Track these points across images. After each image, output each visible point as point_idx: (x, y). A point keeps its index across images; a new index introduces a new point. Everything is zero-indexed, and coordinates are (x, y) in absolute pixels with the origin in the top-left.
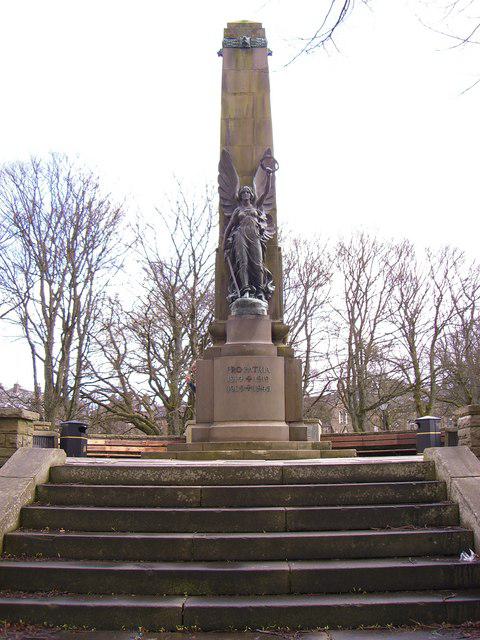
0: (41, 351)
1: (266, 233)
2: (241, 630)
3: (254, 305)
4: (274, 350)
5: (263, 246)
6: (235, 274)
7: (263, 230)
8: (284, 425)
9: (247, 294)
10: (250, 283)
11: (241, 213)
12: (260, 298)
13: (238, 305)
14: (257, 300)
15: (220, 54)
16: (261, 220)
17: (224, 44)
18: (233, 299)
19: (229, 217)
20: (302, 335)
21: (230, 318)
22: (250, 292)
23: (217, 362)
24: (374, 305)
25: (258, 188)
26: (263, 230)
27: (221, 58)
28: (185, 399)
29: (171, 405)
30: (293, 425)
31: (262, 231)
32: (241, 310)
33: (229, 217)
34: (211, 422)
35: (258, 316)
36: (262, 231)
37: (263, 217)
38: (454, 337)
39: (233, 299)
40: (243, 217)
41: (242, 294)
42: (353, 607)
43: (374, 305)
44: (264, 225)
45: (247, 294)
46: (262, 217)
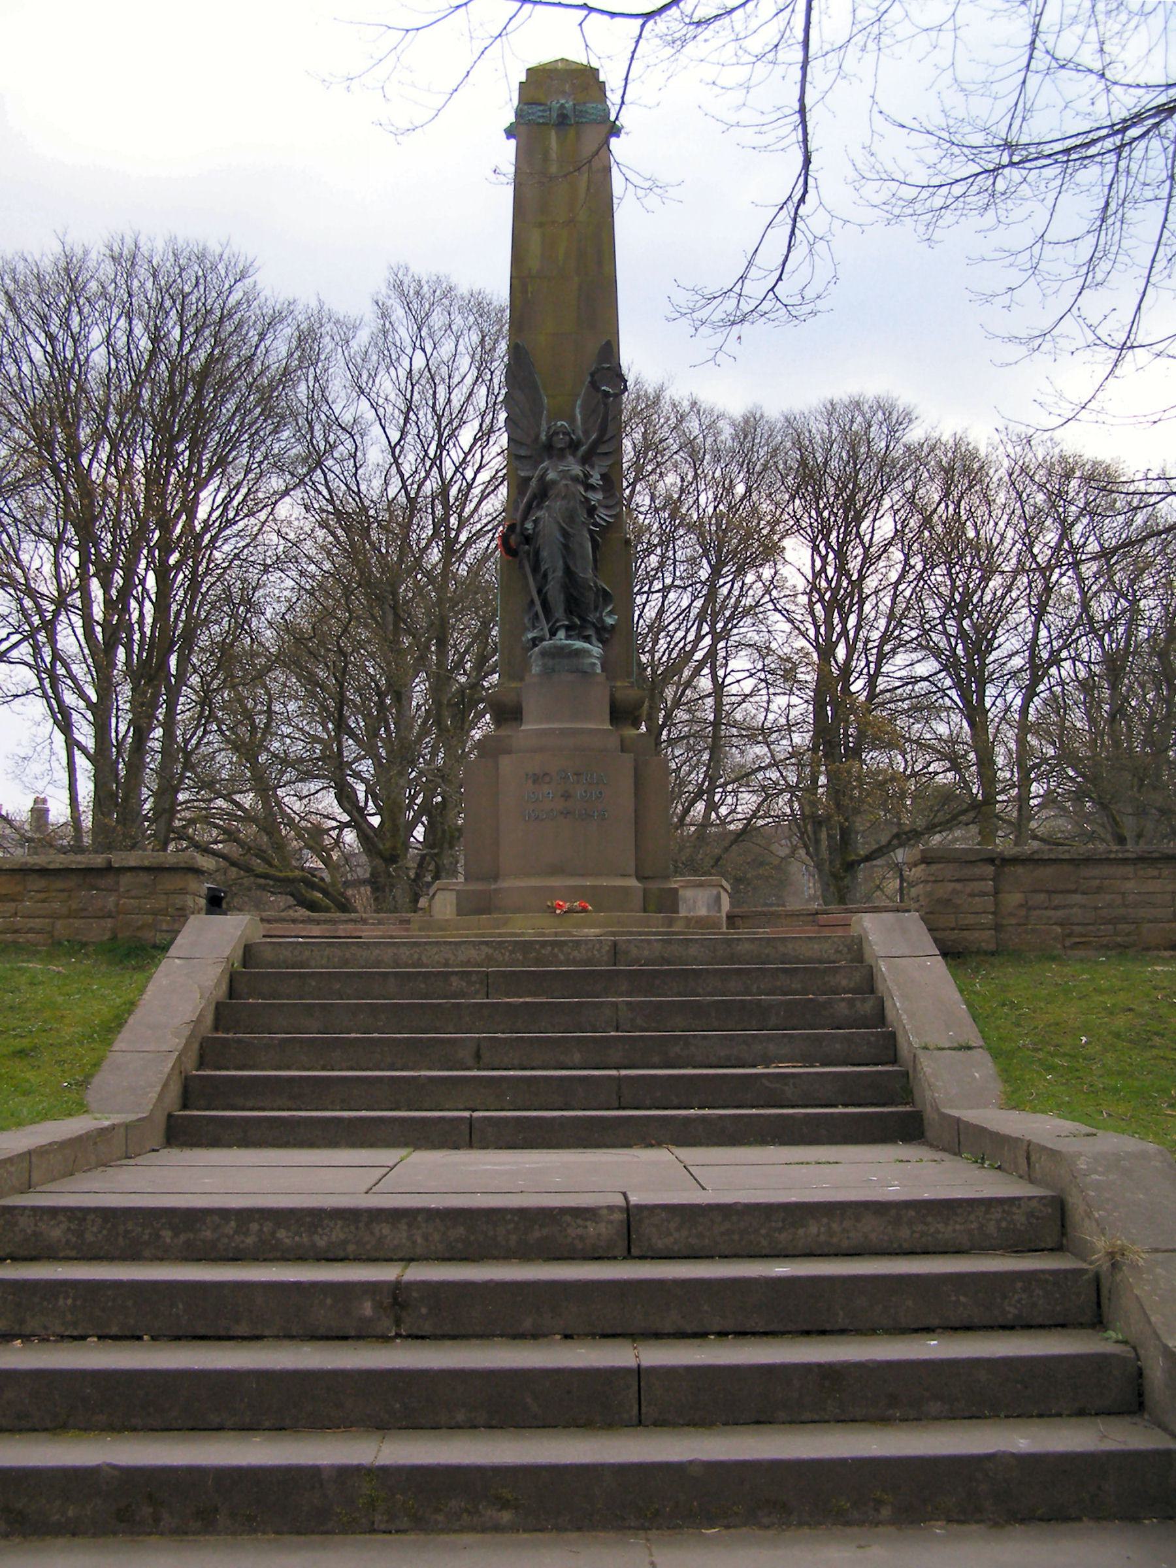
0: (85, 734)
1: (602, 512)
2: (518, 1531)
3: (578, 653)
4: (613, 742)
5: (593, 540)
6: (539, 592)
7: (594, 508)
8: (633, 882)
9: (561, 634)
10: (569, 611)
11: (551, 475)
12: (587, 639)
13: (544, 654)
14: (579, 644)
15: (510, 133)
16: (590, 487)
17: (519, 114)
18: (535, 642)
19: (527, 480)
20: (705, 683)
21: (528, 679)
22: (568, 628)
23: (505, 762)
24: (877, 609)
25: (584, 421)
26: (594, 508)
27: (513, 142)
28: (419, 833)
29: (384, 846)
30: (654, 885)
31: (591, 511)
32: (550, 663)
33: (527, 480)
34: (496, 878)
35: (585, 674)
36: (591, 511)
37: (596, 479)
38: (1086, 686)
39: (535, 642)
40: (554, 482)
41: (553, 633)
42: (707, 1075)
43: (877, 609)
44: (596, 497)
45: (561, 634)
46: (592, 481)
